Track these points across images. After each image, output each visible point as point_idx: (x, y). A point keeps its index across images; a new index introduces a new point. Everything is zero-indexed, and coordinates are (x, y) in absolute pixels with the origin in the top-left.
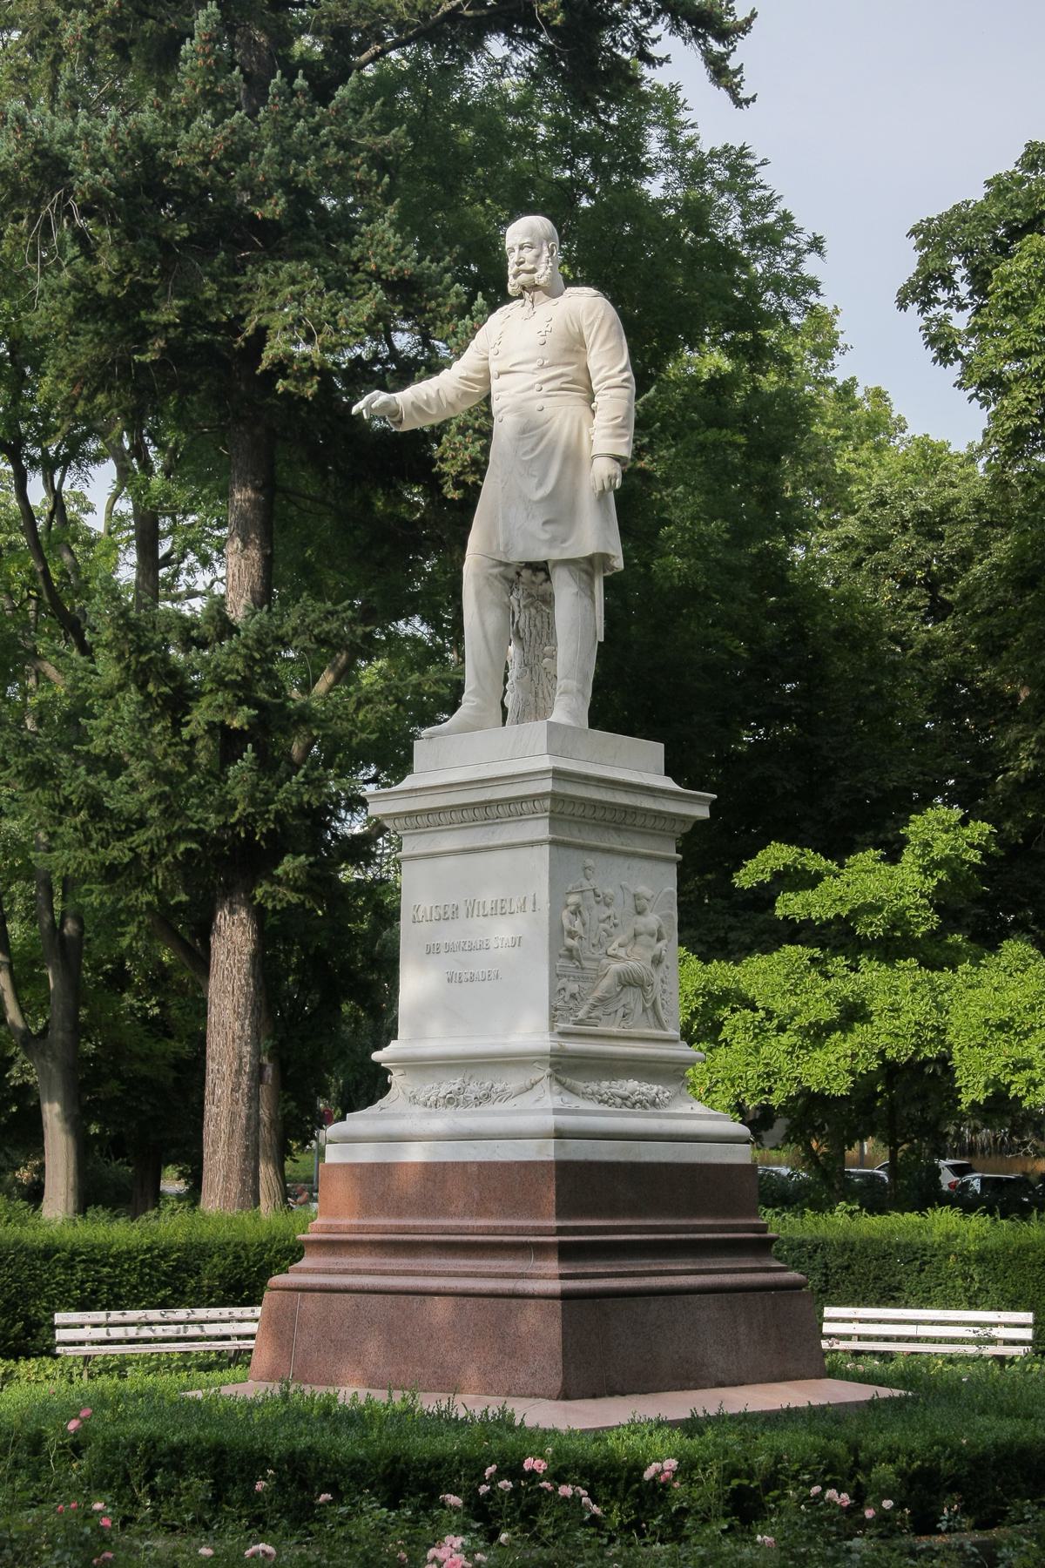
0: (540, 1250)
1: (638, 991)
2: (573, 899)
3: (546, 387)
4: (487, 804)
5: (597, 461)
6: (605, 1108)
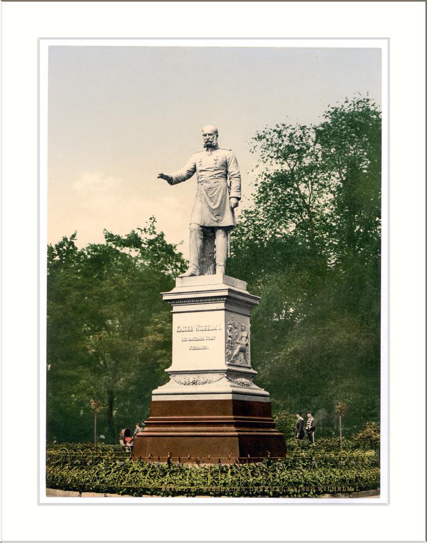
1: (243, 353)
2: (230, 326)
3: (217, 176)
4: (200, 298)
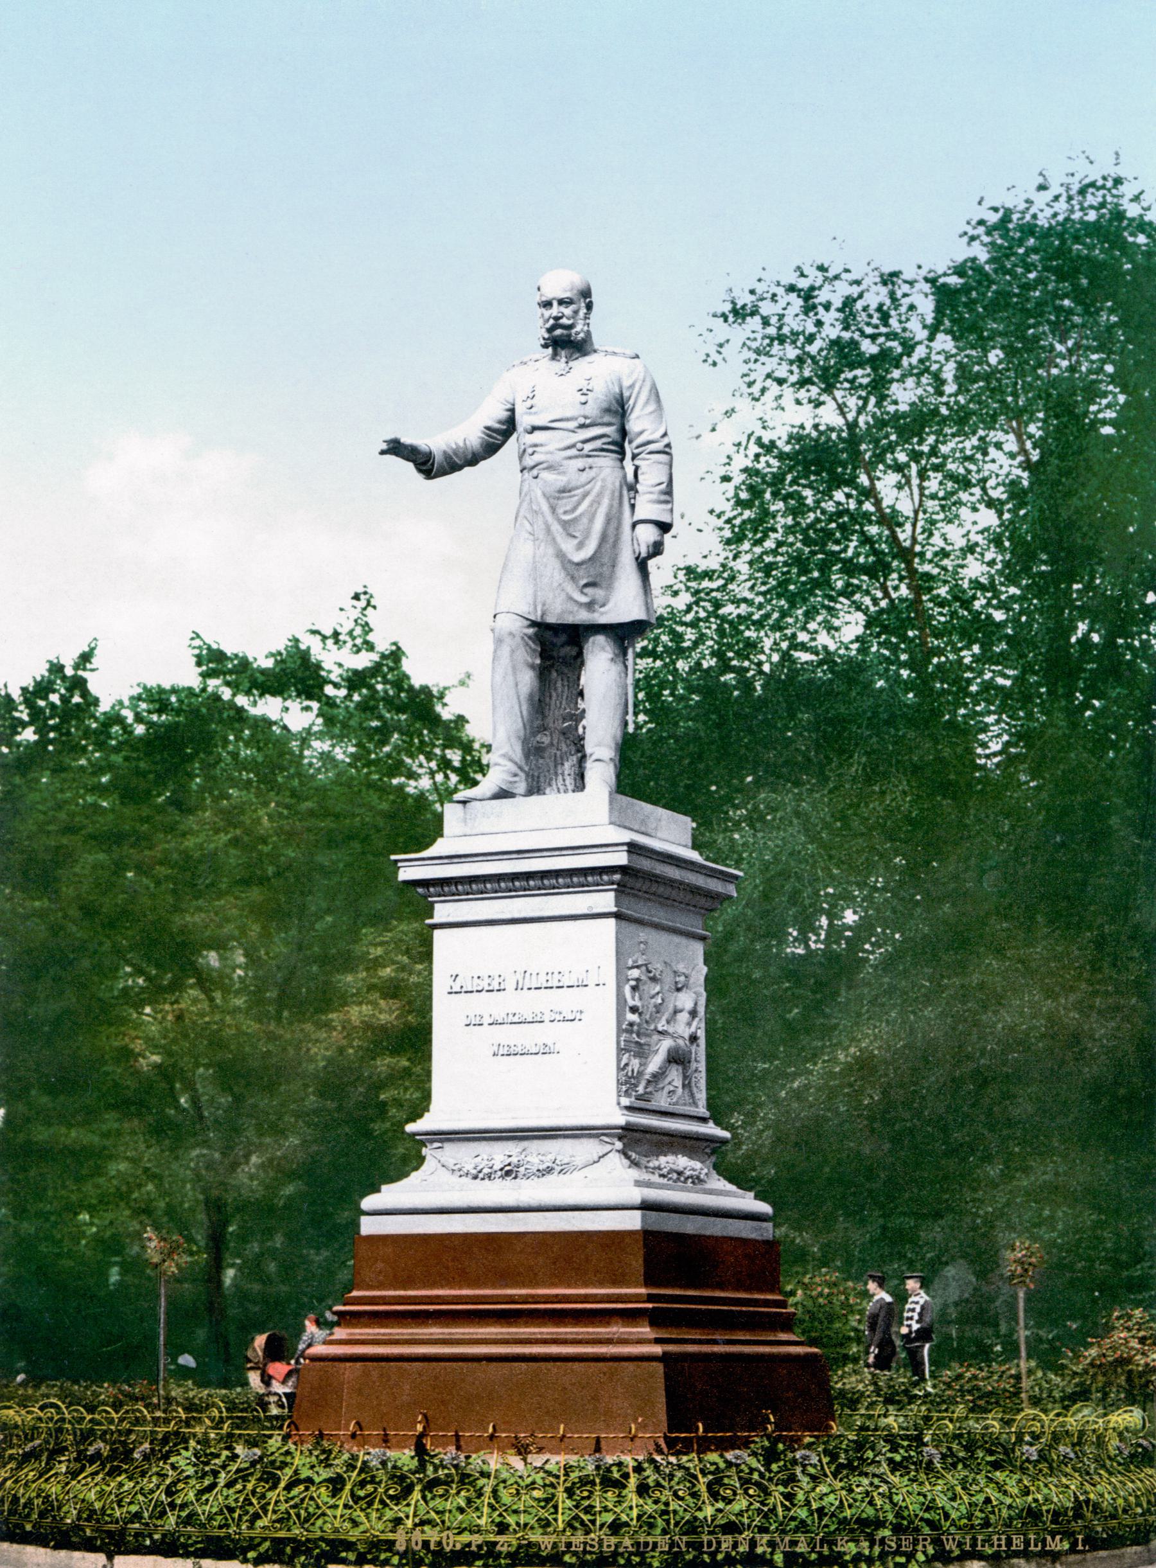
0: (630, 1316)
2: (635, 973)
3: (588, 447)
5: (639, 527)
6: (665, 1181)
